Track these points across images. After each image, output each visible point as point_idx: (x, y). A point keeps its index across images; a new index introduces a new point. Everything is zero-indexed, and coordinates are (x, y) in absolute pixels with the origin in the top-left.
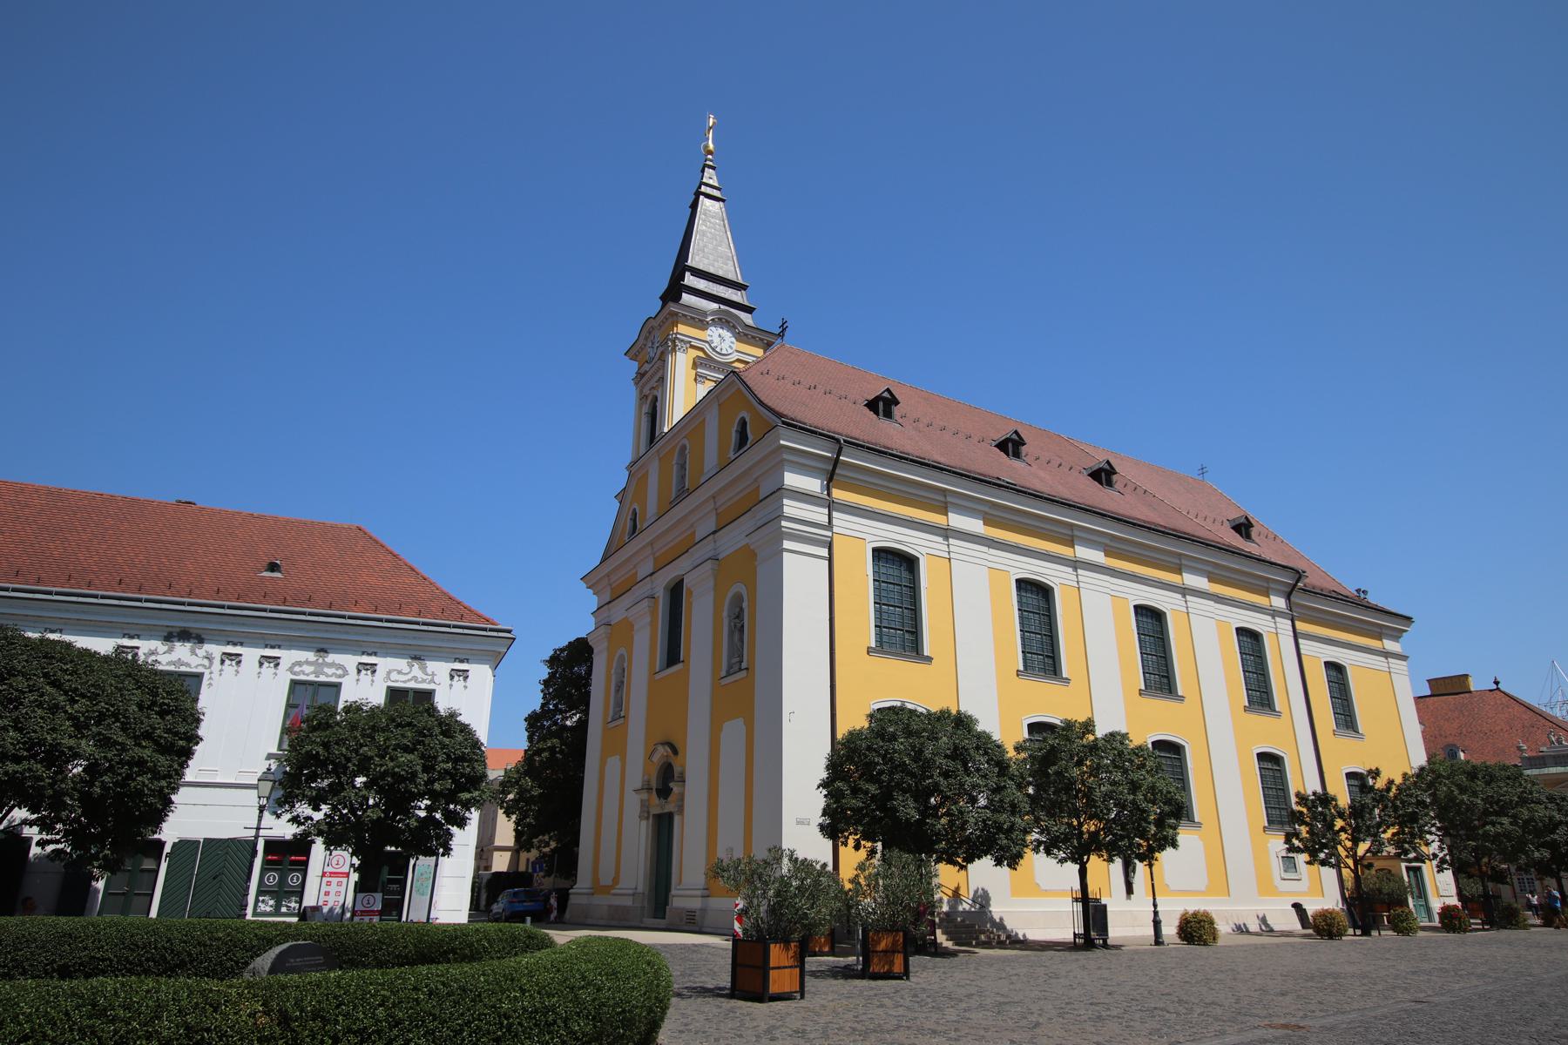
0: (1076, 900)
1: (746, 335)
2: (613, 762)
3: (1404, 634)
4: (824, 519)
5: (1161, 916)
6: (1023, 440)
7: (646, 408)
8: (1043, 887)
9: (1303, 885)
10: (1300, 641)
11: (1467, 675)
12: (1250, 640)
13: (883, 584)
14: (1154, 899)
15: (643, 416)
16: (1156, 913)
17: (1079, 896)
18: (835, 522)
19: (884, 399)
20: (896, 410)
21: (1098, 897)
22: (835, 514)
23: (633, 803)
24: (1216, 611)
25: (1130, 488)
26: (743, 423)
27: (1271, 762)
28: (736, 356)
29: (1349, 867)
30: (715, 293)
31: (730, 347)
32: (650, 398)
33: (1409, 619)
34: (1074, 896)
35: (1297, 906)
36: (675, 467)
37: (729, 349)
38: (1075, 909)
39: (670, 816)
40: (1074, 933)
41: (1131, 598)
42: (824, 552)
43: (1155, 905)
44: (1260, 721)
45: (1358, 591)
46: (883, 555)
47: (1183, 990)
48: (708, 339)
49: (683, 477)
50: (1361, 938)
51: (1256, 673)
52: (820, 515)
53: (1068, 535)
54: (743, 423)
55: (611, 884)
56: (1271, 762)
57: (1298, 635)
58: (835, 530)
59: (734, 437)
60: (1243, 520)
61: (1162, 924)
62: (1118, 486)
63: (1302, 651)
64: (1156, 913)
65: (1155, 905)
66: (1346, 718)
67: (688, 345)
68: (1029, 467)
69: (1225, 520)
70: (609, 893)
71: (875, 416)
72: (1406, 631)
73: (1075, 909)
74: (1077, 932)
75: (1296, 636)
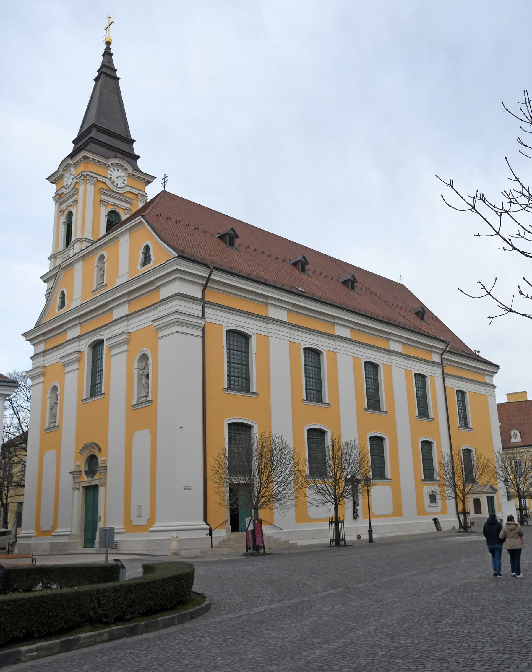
0: (331, 522)
1: (134, 175)
2: (50, 456)
3: (495, 374)
4: (200, 314)
5: (372, 528)
6: (307, 262)
7: (63, 219)
8: (312, 517)
9: (439, 509)
10: (446, 379)
11: (526, 392)
12: (421, 378)
13: (231, 351)
14: (370, 520)
15: (61, 224)
16: (370, 527)
17: (334, 520)
18: (206, 315)
19: (229, 234)
20: (237, 241)
21: (331, 524)
22: (207, 310)
23: (67, 480)
24: (406, 365)
25: (364, 289)
26: (147, 248)
27: (427, 445)
28: (127, 189)
29: (461, 499)
30: (110, 138)
31: (123, 183)
32: (66, 212)
33: (498, 367)
34: (330, 521)
35: (435, 520)
36: (96, 268)
37: (122, 185)
38: (331, 528)
39: (96, 487)
40: (330, 539)
41: (363, 358)
42: (200, 333)
43: (370, 523)
44: (424, 422)
45: (475, 351)
46: (232, 334)
47: (336, 622)
48: (109, 176)
49: (102, 276)
50: (125, 165)
51: (424, 408)
52: (197, 310)
53: (521, 661)
54: (147, 248)
55: (50, 529)
56: (427, 445)
57: (444, 374)
58: (207, 320)
59: (141, 257)
60: (420, 310)
61: (373, 532)
62: (357, 289)
63: (446, 385)
64: (370, 527)
65: (370, 523)
66: (464, 422)
67: (96, 180)
68: (310, 278)
69: (412, 309)
70: (50, 535)
71: (224, 245)
72: (496, 373)
73: (331, 528)
74: (331, 539)
75: (443, 374)
